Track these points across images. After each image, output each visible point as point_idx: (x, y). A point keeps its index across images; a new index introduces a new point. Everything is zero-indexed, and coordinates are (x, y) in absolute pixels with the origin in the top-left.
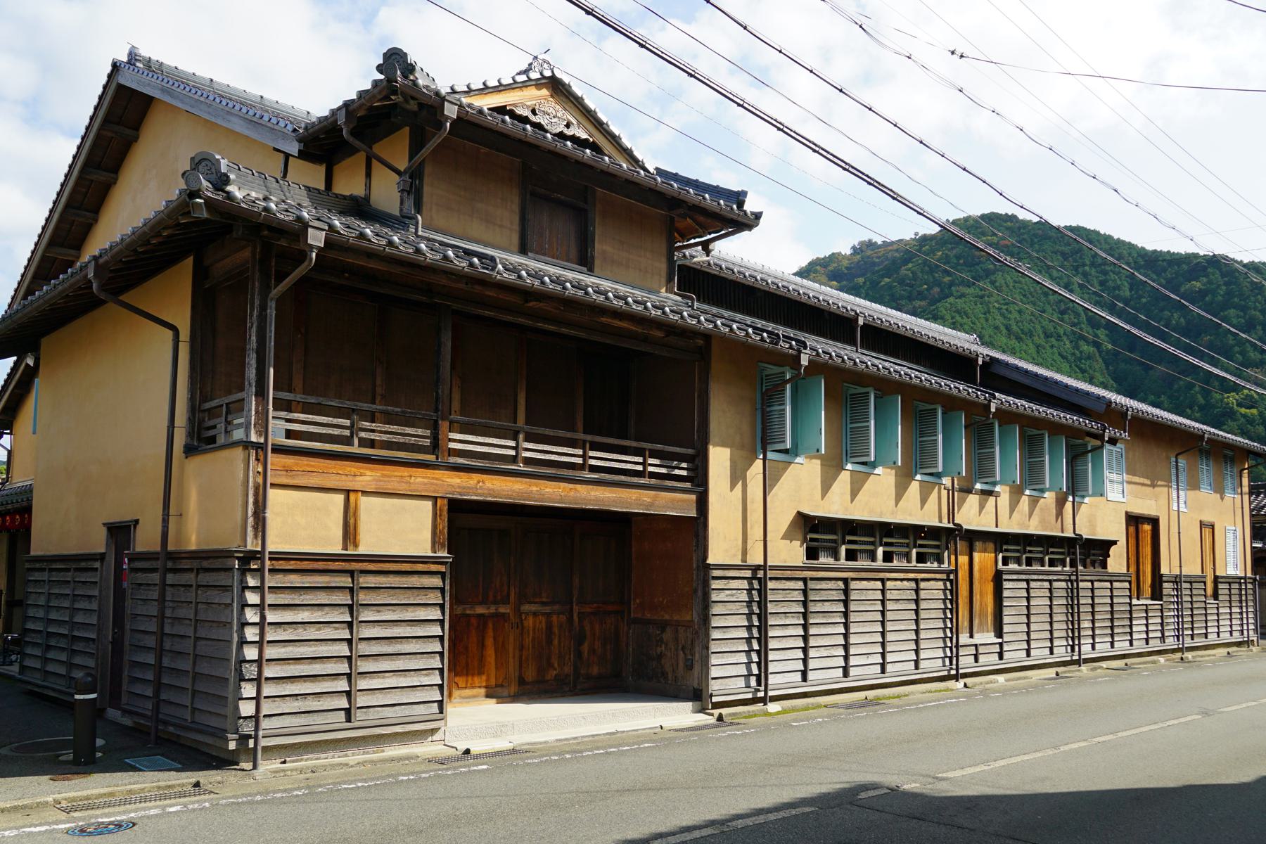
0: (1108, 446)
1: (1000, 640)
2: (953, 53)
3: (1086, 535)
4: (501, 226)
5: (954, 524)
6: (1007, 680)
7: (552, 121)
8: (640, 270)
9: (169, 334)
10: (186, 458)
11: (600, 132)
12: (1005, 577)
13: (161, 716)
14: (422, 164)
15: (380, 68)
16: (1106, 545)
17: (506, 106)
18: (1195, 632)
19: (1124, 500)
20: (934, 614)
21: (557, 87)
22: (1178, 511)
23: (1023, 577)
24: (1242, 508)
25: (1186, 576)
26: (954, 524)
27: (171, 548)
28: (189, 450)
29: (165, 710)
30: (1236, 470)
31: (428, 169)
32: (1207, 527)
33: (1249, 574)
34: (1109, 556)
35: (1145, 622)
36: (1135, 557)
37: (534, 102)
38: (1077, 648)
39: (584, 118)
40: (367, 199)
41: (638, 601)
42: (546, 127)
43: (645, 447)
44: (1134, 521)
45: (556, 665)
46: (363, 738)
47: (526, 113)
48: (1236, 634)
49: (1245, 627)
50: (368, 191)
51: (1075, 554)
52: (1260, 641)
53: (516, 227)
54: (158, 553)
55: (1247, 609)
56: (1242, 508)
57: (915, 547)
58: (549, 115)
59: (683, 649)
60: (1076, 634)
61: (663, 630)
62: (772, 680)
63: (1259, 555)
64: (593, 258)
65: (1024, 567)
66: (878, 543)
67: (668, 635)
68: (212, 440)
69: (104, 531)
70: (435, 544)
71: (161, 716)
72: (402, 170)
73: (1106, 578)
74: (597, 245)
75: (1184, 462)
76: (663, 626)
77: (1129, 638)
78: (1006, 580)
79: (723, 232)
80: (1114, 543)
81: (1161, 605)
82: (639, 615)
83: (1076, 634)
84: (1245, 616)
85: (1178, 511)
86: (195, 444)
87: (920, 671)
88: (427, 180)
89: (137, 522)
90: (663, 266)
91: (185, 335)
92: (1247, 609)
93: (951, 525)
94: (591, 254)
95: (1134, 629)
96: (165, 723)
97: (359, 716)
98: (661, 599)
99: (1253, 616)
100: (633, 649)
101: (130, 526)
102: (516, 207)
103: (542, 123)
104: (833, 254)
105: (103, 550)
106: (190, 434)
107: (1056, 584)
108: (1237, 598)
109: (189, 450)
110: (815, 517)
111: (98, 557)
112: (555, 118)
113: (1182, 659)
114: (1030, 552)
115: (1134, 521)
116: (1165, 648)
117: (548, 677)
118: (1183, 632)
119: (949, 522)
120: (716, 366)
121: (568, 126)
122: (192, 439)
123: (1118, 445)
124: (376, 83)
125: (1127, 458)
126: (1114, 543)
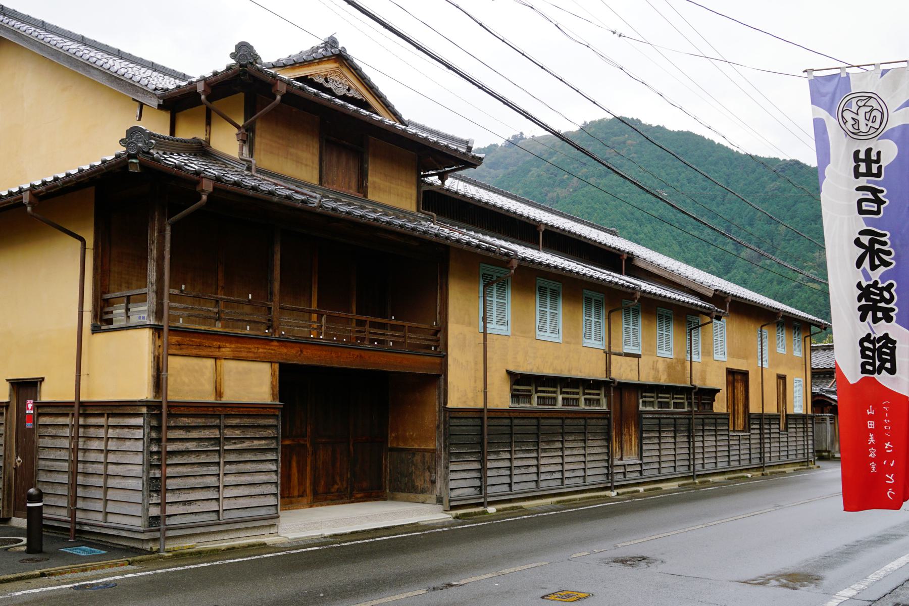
0: (714, 321)
1: (640, 462)
2: (614, 33)
3: (698, 383)
4: (306, 165)
5: (610, 379)
6: (645, 490)
7: (339, 86)
8: (398, 195)
9: (79, 243)
10: (93, 334)
11: (363, 85)
12: (644, 416)
13: (77, 520)
14: (254, 122)
15: (233, 56)
16: (714, 392)
17: (307, 76)
18: (772, 455)
19: (725, 360)
20: (683, 451)
21: (342, 59)
22: (762, 367)
23: (657, 416)
24: (805, 365)
25: (766, 415)
26: (610, 379)
27: (82, 399)
28: (96, 330)
29: (80, 515)
30: (802, 336)
31: (258, 126)
32: (782, 378)
33: (810, 413)
34: (714, 400)
35: (727, 443)
36: (732, 400)
37: (326, 73)
38: (692, 467)
39: (362, 86)
40: (208, 141)
41: (393, 435)
42: (334, 90)
43: (404, 324)
44: (731, 372)
45: (338, 481)
46: (592, 489)
47: (322, 81)
48: (800, 456)
49: (806, 451)
50: (208, 136)
51: (691, 399)
52: (175, 363)
53: (317, 166)
54: (74, 402)
55: (807, 438)
56: (805, 365)
57: (584, 395)
58: (336, 82)
59: (429, 468)
60: (692, 457)
61: (414, 454)
62: (490, 490)
63: (817, 398)
64: (367, 187)
65: (656, 409)
66: (559, 392)
67: (418, 458)
68: (110, 322)
69: (7, 386)
70: (274, 399)
71: (77, 520)
72: (241, 126)
73: (713, 416)
74: (370, 178)
75: (766, 331)
76: (414, 452)
77: (727, 460)
78: (645, 418)
79: (455, 167)
80: (718, 391)
81: (749, 435)
82: (395, 445)
83: (692, 457)
84: (806, 447)
85: (762, 367)
86: (99, 324)
87: (643, 477)
88: (258, 132)
89: (43, 379)
90: (413, 192)
91: (90, 243)
92: (807, 438)
93: (608, 379)
94: (366, 184)
95: (731, 453)
96: (80, 524)
97: (566, 482)
98: (411, 433)
99: (811, 434)
100: (390, 470)
101: (37, 382)
102: (316, 152)
103: (332, 88)
104: (491, 145)
105: (7, 400)
106: (95, 316)
107: (679, 421)
108: (721, 238)
109: (96, 330)
110: (518, 374)
111: (5, 405)
112: (341, 83)
113: (763, 475)
114: (661, 398)
115: (731, 372)
116: (752, 467)
117: (333, 490)
118: (764, 455)
119: (607, 377)
120: (452, 264)
121: (349, 90)
122: (96, 321)
123: (722, 319)
124: (229, 68)
125: (727, 329)
126: (718, 391)
